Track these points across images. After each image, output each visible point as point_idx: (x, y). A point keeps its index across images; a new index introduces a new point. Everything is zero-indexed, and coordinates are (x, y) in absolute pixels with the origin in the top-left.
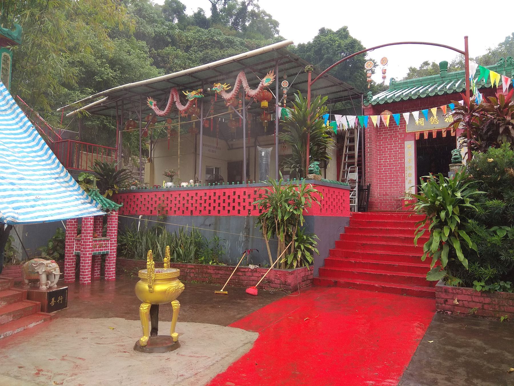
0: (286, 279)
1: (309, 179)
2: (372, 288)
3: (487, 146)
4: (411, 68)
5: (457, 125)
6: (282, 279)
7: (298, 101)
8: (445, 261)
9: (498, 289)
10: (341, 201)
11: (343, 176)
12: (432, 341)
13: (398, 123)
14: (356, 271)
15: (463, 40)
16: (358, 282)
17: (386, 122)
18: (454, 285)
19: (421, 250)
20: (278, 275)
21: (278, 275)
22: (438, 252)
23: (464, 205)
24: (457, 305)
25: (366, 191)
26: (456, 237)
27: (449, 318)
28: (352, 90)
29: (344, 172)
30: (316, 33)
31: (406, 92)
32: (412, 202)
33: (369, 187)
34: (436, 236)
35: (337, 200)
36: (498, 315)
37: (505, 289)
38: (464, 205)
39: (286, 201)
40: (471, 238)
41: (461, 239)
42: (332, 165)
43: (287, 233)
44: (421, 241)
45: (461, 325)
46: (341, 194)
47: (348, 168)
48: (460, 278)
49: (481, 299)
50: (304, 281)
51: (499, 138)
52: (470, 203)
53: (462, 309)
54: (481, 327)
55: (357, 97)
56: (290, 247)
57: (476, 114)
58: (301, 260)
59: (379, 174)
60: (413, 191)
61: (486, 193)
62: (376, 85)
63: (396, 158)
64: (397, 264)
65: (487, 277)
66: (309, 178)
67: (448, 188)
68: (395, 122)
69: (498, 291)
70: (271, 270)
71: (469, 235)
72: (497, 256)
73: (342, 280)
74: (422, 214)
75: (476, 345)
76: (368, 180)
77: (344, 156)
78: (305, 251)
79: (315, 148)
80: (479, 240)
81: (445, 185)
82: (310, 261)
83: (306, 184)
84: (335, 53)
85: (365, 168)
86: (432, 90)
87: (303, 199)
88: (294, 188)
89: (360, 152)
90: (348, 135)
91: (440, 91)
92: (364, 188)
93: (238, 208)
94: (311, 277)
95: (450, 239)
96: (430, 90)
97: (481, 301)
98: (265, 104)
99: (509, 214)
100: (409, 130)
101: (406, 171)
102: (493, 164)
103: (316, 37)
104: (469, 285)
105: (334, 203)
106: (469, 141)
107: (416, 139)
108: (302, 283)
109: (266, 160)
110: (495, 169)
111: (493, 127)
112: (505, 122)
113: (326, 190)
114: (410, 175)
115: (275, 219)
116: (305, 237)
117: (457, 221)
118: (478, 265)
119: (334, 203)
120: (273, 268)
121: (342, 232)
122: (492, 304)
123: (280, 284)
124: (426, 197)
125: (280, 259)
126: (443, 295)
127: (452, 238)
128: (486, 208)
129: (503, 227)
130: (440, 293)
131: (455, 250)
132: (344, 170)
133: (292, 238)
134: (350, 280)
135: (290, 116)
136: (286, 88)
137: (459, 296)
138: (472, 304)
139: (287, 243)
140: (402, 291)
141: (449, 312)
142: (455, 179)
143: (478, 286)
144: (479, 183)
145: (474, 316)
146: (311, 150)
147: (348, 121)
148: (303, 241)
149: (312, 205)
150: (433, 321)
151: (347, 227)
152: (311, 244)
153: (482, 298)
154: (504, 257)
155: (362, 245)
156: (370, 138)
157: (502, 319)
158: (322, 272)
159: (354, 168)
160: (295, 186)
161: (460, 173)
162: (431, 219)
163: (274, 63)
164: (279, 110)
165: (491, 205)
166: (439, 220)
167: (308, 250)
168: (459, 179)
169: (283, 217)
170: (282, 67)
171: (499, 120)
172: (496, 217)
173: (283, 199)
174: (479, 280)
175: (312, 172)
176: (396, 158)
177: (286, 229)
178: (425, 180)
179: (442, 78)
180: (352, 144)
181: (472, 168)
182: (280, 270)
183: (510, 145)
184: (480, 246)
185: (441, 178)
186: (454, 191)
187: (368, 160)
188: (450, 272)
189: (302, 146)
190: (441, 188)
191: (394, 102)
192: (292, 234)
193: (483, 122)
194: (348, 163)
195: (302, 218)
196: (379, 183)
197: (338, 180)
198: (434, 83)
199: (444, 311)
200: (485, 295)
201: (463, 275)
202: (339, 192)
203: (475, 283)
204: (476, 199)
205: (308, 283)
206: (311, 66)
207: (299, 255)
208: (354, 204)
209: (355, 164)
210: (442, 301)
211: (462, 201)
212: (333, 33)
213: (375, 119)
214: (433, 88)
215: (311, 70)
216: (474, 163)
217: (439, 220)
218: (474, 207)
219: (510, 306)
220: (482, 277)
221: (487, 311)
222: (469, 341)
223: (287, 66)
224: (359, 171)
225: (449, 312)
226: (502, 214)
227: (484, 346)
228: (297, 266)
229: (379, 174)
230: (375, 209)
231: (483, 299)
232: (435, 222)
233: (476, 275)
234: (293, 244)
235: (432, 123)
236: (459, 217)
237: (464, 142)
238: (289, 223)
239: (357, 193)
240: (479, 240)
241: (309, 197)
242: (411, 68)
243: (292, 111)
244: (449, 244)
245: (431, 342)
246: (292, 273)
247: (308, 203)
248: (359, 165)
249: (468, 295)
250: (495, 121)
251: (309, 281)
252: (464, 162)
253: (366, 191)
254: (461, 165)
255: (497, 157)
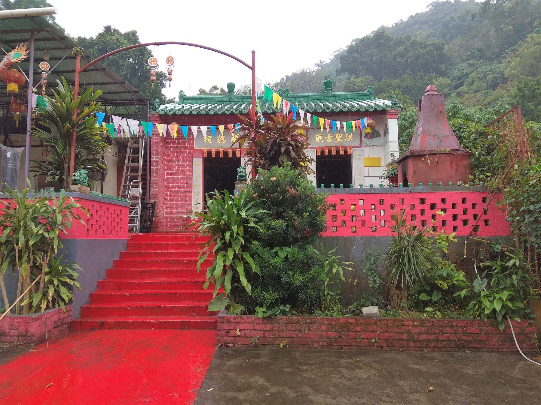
0: (27, 329)
1: (71, 191)
2: (147, 325)
3: (271, 165)
4: (201, 89)
5: (243, 141)
6: (22, 329)
7: (61, 90)
8: (228, 287)
9: (278, 314)
10: (117, 220)
11: (124, 191)
12: (212, 389)
13: (186, 135)
14: (128, 306)
15: (251, 54)
16: (131, 319)
17: (173, 133)
18: (236, 314)
19: (203, 274)
20: (15, 324)
21: (15, 324)
22: (222, 278)
23: (249, 225)
24: (239, 336)
25: (150, 210)
26: (239, 259)
27: (231, 352)
28: (136, 94)
29: (125, 187)
30: (101, 30)
31: (195, 106)
32: (199, 221)
33: (154, 205)
34: (220, 260)
35: (111, 219)
36: (277, 342)
37: (284, 313)
38: (249, 225)
39: (34, 219)
40: (254, 260)
41: (245, 261)
42: (111, 177)
43: (34, 263)
44: (206, 264)
45: (243, 359)
46: (118, 212)
47: (130, 182)
48: (242, 305)
49: (263, 326)
50: (58, 327)
51: (281, 158)
52: (254, 222)
53: (244, 340)
54: (262, 360)
55: (142, 102)
56: (38, 283)
57: (261, 131)
58: (54, 299)
59: (165, 191)
60: (200, 210)
61: (269, 212)
62: (167, 100)
63: (184, 175)
64: (178, 292)
65: (269, 301)
66: (73, 189)
67: (233, 206)
68: (184, 137)
69: (278, 316)
70: (4, 317)
71: (253, 257)
72: (278, 278)
73: (110, 320)
74: (207, 235)
75: (258, 384)
76: (153, 197)
77: (125, 168)
78: (60, 286)
79: (84, 152)
80: (262, 263)
81: (230, 203)
82: (67, 299)
83: (64, 198)
84: (122, 56)
85: (150, 184)
86: (220, 108)
87: (59, 218)
88: (47, 202)
89: (144, 165)
90: (131, 144)
91: (227, 110)
92: (148, 206)
93: (465, 206)
94: (68, 320)
95: (234, 263)
96: (218, 108)
97: (262, 329)
98: (13, 87)
99: (290, 234)
100: (197, 146)
101: (194, 189)
102: (276, 183)
103: (100, 34)
104: (251, 311)
105: (108, 223)
106: (253, 159)
107: (204, 157)
108: (53, 330)
109: (13, 163)
110: (277, 187)
111: (276, 145)
112: (286, 142)
113: (97, 206)
114: (197, 194)
115: (15, 245)
116: (60, 268)
117: (242, 242)
118: (261, 290)
119: (108, 223)
120: (9, 313)
121: (117, 258)
122: (273, 330)
123: (18, 336)
124: (211, 216)
125: (22, 300)
126: (225, 327)
127: (236, 261)
128: (269, 228)
129: (284, 248)
130: (222, 324)
131: (238, 274)
132: (126, 185)
133: (41, 270)
134: (121, 319)
135: (49, 108)
136: (45, 71)
137: (241, 325)
138: (253, 333)
139: (34, 277)
140: (183, 325)
141: (230, 345)
142: (240, 197)
143: (260, 312)
144: (262, 202)
145: (256, 346)
146: (77, 156)
147: (128, 126)
148: (58, 274)
149: (73, 225)
150: (214, 360)
151: (124, 251)
152: (70, 277)
153: (263, 326)
154: (285, 280)
155: (141, 272)
156: (157, 151)
157: (282, 345)
158: (85, 311)
159: (137, 182)
160: (50, 199)
161: (245, 191)
162: (216, 240)
163: (28, 35)
164: (33, 99)
165: (273, 225)
166: (223, 241)
167: (65, 284)
168: (244, 197)
169: (27, 241)
170: (42, 44)
171: (281, 140)
172: (278, 238)
173: (29, 216)
174: (261, 306)
175: (76, 182)
176: (184, 175)
177: (32, 258)
178: (211, 197)
179: (229, 99)
180: (135, 155)
181: (257, 186)
182: (21, 316)
183: (291, 165)
184: (263, 269)
185: (227, 195)
186: (239, 210)
187: (153, 174)
188: (233, 299)
189: (64, 148)
190: (226, 206)
191: (182, 115)
192: (41, 265)
193: (267, 141)
194: (130, 176)
195: (56, 243)
196: (166, 201)
197: (118, 196)
198: (222, 103)
199: (226, 345)
200: (266, 322)
201: (245, 302)
202: (115, 210)
203: (258, 309)
204: (259, 219)
205: (63, 329)
206: (81, 49)
207: (51, 292)
208: (136, 224)
209: (139, 179)
210: (224, 333)
211: (247, 221)
212: (121, 35)
213: (161, 128)
214: (220, 106)
215: (81, 54)
216: (258, 182)
217: (223, 241)
218: (258, 227)
219: (289, 331)
220: (264, 302)
221: (267, 339)
222: (251, 380)
223: (49, 44)
224: (143, 186)
225: (230, 345)
226: (284, 234)
227: (267, 384)
228: (48, 307)
229: (165, 191)
230: (161, 230)
231: (264, 326)
232: (219, 243)
233: (258, 300)
234: (42, 278)
235: (220, 142)
236: (243, 238)
237: (249, 160)
238: (39, 250)
239: (139, 211)
240: (262, 263)
241: (69, 214)
242: (201, 89)
243: (52, 102)
244: (233, 267)
245: (210, 390)
246: (37, 319)
247: (67, 222)
248: (144, 179)
249: (250, 323)
250: (278, 140)
251: (65, 325)
252: (249, 181)
253: (150, 210)
254: (246, 183)
255: (280, 175)
